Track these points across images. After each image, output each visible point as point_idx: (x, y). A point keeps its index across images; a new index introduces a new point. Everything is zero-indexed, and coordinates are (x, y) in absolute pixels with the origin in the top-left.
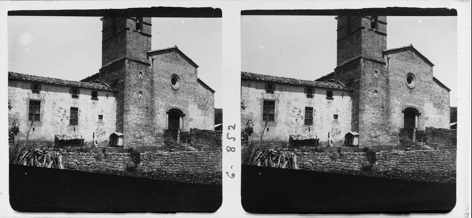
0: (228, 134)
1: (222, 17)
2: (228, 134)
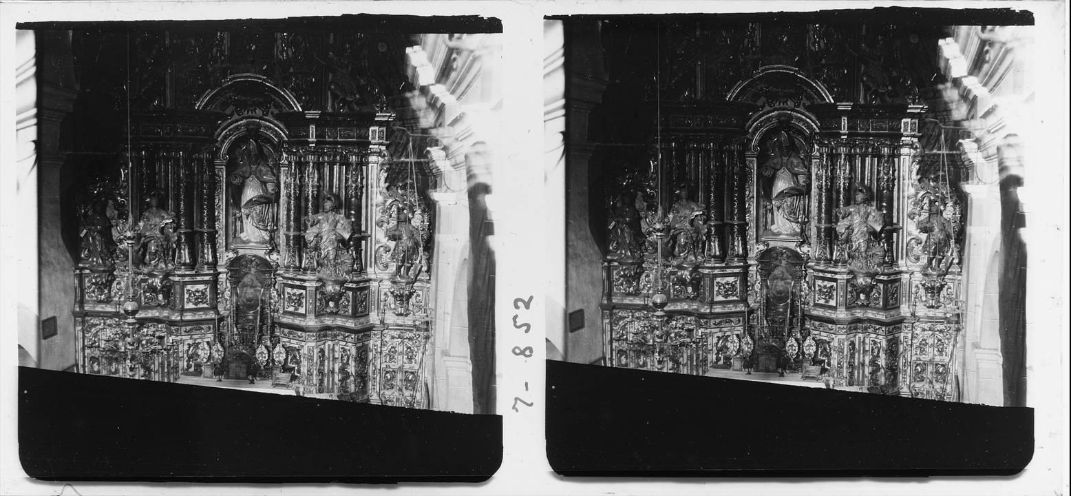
0: (516, 317)
1: (1033, 24)
2: (516, 317)
